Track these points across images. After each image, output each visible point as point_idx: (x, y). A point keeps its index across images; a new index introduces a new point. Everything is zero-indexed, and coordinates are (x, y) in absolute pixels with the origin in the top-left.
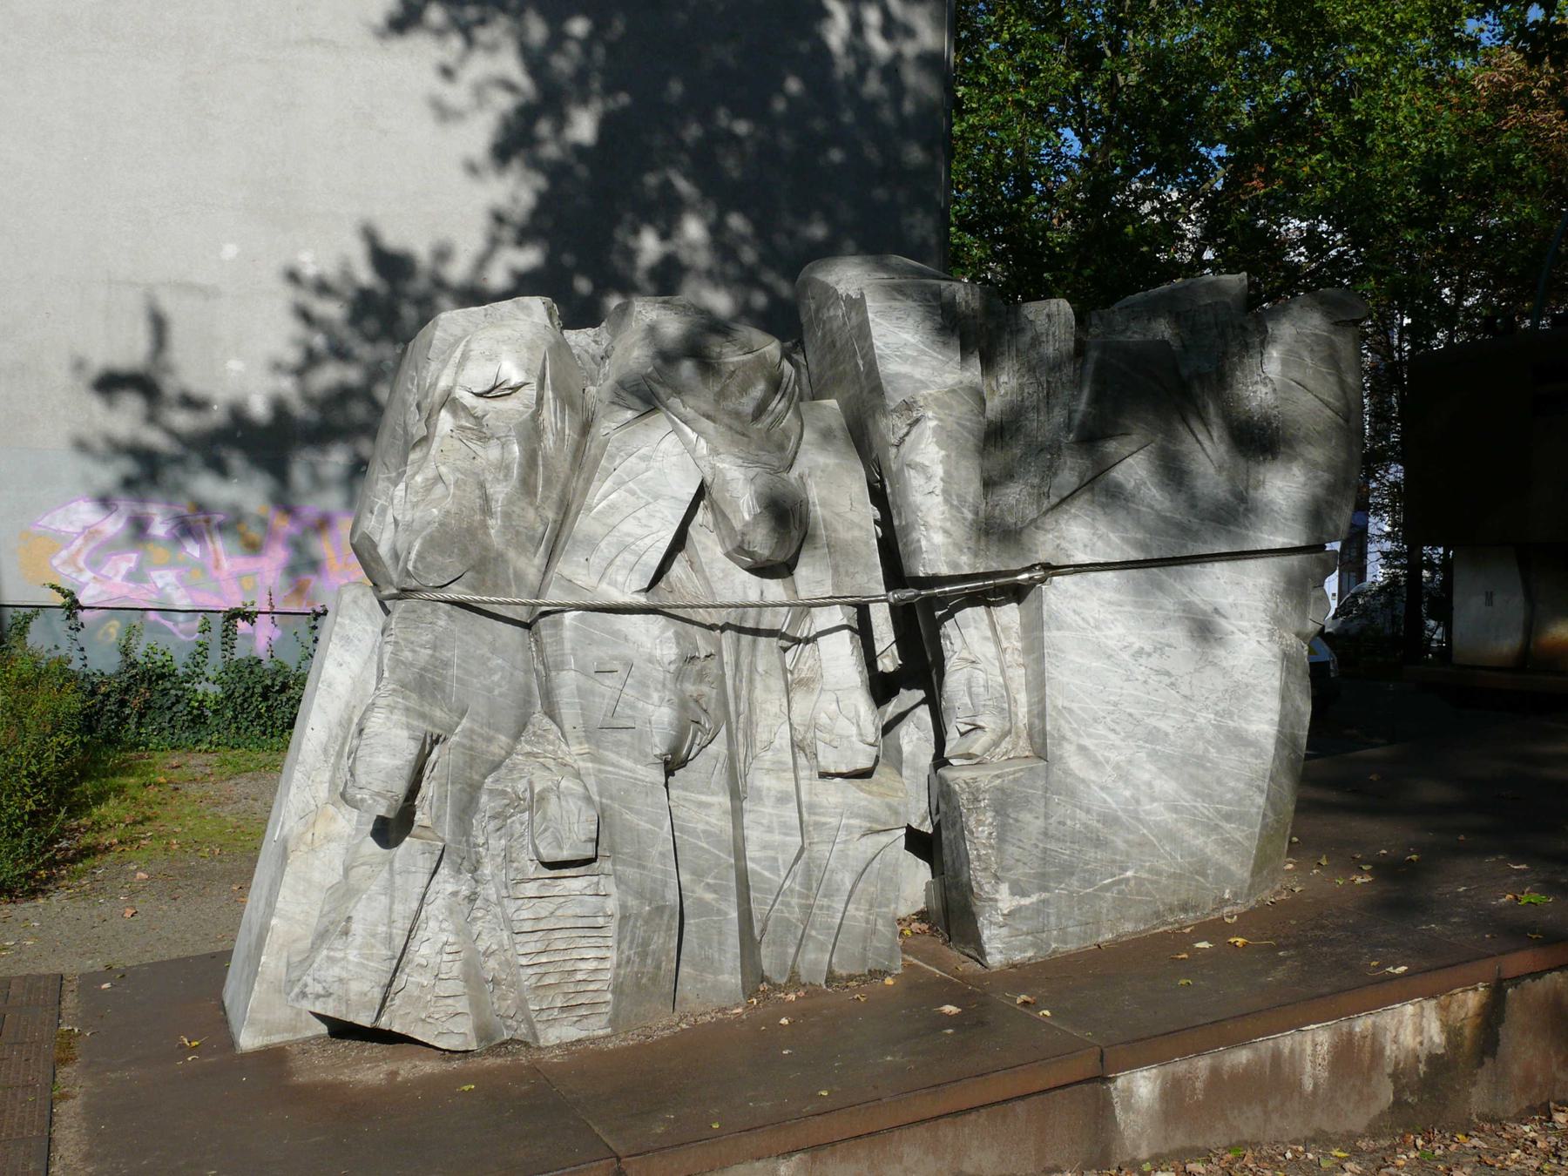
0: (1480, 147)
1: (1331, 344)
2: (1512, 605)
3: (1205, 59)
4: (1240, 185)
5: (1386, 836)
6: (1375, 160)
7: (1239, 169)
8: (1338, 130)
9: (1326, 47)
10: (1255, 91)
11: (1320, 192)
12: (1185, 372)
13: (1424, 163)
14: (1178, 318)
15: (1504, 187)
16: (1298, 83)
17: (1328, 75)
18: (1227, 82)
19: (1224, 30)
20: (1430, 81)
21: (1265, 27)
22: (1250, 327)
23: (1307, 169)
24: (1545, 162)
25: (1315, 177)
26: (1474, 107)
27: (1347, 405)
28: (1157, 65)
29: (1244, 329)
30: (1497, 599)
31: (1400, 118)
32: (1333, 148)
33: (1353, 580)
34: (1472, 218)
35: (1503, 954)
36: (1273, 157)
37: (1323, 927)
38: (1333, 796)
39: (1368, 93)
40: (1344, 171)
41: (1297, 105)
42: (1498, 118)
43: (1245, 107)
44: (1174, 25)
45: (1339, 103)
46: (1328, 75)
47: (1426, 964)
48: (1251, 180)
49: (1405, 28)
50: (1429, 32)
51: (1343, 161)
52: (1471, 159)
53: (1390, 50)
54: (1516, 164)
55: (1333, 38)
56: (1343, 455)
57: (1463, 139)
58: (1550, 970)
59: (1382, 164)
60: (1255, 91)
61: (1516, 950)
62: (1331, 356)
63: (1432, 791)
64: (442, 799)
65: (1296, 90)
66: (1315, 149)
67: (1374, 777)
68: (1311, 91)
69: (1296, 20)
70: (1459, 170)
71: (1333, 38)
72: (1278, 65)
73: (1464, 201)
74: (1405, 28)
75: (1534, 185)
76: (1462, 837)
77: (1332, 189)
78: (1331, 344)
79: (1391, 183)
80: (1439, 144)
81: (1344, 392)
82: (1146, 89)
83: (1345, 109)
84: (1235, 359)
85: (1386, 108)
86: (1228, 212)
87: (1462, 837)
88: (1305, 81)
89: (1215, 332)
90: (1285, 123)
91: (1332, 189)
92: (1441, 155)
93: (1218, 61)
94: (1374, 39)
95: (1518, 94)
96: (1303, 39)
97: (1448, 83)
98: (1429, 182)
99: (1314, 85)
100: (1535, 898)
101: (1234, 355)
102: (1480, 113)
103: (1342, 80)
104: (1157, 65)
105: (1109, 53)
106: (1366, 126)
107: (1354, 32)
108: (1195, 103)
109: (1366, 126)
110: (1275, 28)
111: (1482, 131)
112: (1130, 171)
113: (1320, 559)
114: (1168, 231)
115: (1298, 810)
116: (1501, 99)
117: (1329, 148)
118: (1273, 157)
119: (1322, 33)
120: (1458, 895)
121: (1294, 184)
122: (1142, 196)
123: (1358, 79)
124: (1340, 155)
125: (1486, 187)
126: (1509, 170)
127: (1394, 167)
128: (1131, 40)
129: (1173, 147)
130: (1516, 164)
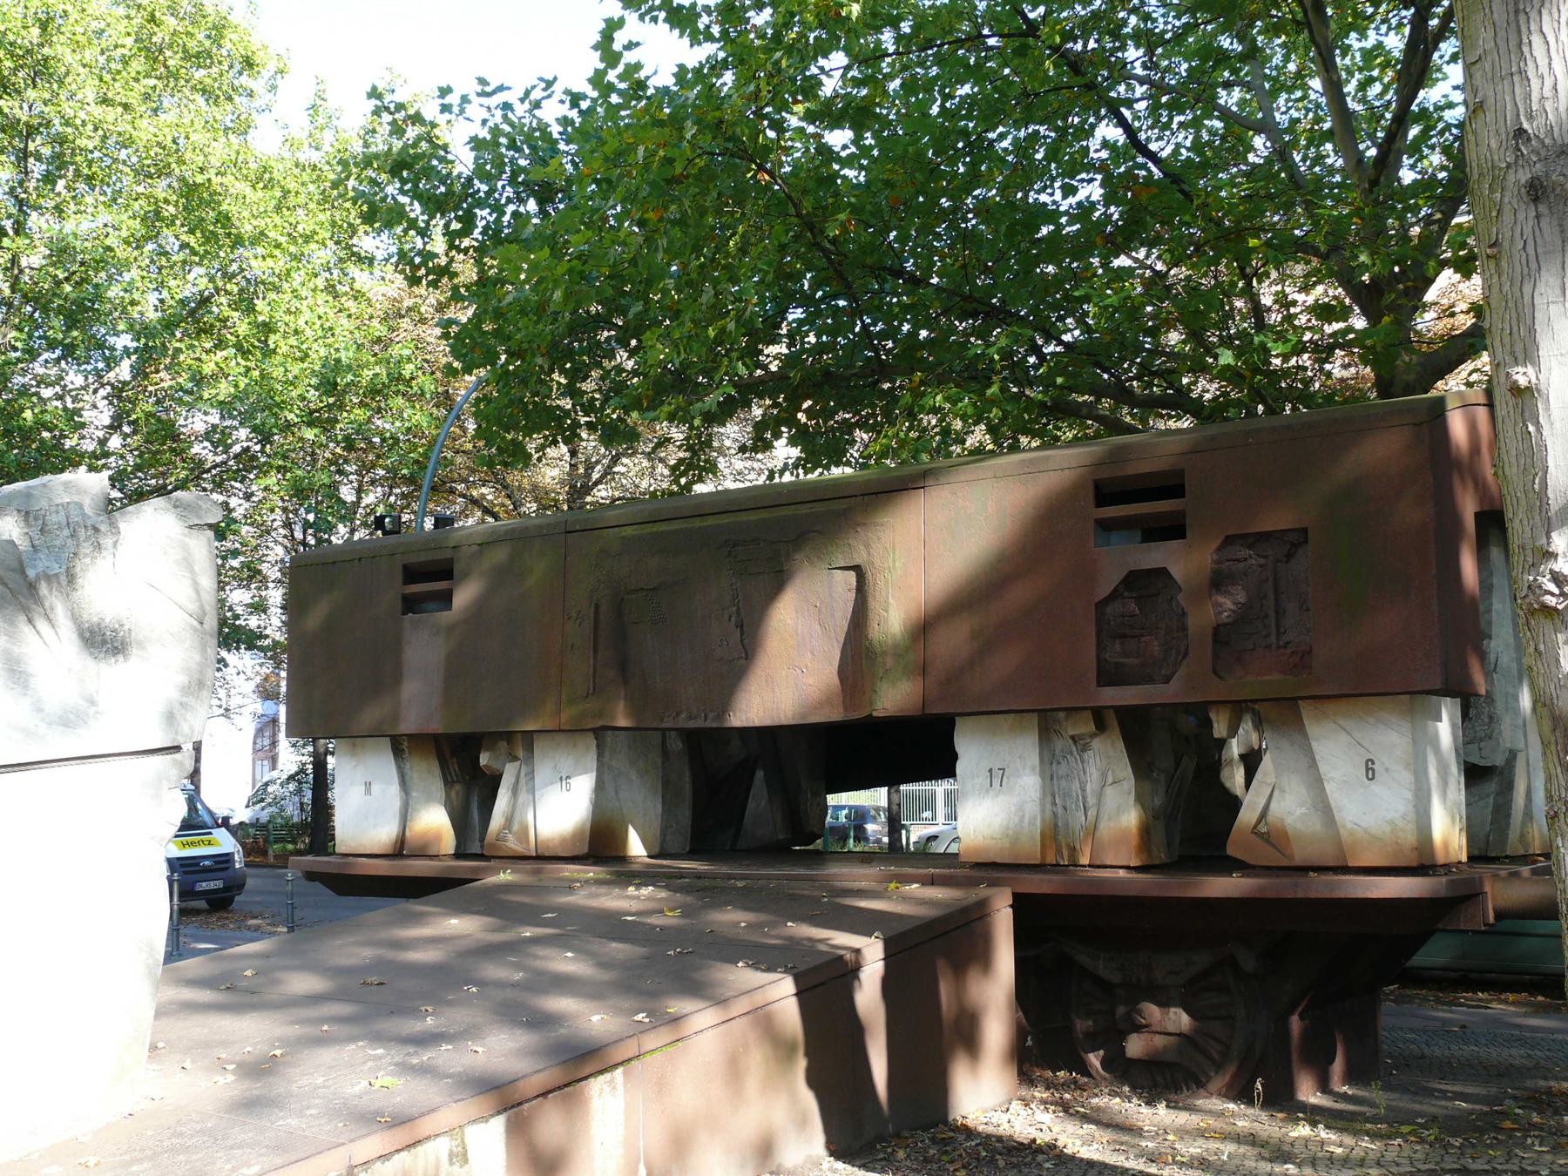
0: (375, 355)
1: (185, 548)
2: (388, 791)
3: (109, 249)
4: (146, 376)
5: (252, 1032)
6: (278, 359)
7: (146, 360)
8: (243, 328)
9: (232, 248)
10: (161, 285)
11: (224, 389)
12: (31, 573)
13: (323, 366)
14: (26, 515)
15: (397, 393)
16: (205, 280)
17: (234, 276)
18: (135, 273)
19: (131, 222)
20: (330, 288)
21: (173, 223)
22: (103, 528)
23: (212, 365)
24: (433, 373)
25: (221, 373)
26: (371, 317)
27: (202, 607)
28: (61, 252)
29: (97, 530)
30: (375, 788)
31: (301, 322)
32: (239, 347)
33: (266, 768)
34: (369, 420)
35: (352, 1141)
36: (178, 351)
37: (181, 1135)
38: (205, 996)
39: (272, 296)
40: (248, 369)
41: (204, 301)
42: (392, 329)
43: (153, 298)
44: (79, 212)
45: (245, 303)
46: (234, 276)
47: (279, 1161)
48: (157, 372)
49: (307, 239)
50: (330, 243)
51: (247, 359)
52: (366, 365)
53: (294, 257)
54: (407, 374)
55: (238, 241)
56: (197, 657)
57: (359, 347)
58: (398, 1151)
59: (283, 364)
60: (161, 285)
61: (368, 1135)
62: (185, 559)
63: (302, 983)
64: (745, 899)
65: (202, 287)
66: (220, 345)
67: (248, 973)
68: (217, 290)
69: (203, 220)
70: (355, 375)
71: (238, 241)
72: (184, 262)
73: (362, 404)
74: (307, 239)
75: (423, 394)
76: (325, 1028)
77: (236, 386)
78: (185, 548)
79: (292, 384)
80: (337, 350)
81: (198, 592)
82: (47, 273)
83: (251, 309)
84: (88, 560)
85: (289, 312)
86: (134, 402)
87: (325, 1028)
88: (212, 279)
89: (66, 532)
90: (194, 317)
91: (236, 386)
92: (338, 361)
93: (122, 252)
94: (278, 246)
95: (409, 309)
96: (210, 238)
97: (346, 294)
98: (328, 386)
99: (220, 284)
100: (388, 1081)
101: (86, 555)
102: (375, 323)
103: (248, 281)
104: (61, 252)
105: (11, 233)
106: (268, 328)
107: (260, 237)
108: (98, 296)
109: (268, 328)
110: (182, 225)
111: (379, 340)
112: (32, 354)
113: (175, 761)
114: (73, 420)
115: (159, 1014)
116: (394, 315)
117: (234, 346)
118: (178, 351)
119: (229, 235)
120: (317, 1087)
121: (199, 380)
122: (42, 381)
123: (263, 283)
124: (245, 353)
125: (379, 392)
126: (399, 378)
127: (295, 369)
128: (34, 220)
129: (75, 333)
130: (407, 374)
